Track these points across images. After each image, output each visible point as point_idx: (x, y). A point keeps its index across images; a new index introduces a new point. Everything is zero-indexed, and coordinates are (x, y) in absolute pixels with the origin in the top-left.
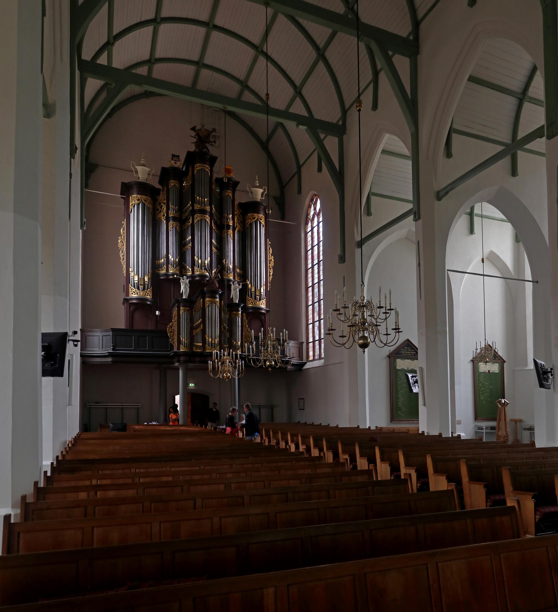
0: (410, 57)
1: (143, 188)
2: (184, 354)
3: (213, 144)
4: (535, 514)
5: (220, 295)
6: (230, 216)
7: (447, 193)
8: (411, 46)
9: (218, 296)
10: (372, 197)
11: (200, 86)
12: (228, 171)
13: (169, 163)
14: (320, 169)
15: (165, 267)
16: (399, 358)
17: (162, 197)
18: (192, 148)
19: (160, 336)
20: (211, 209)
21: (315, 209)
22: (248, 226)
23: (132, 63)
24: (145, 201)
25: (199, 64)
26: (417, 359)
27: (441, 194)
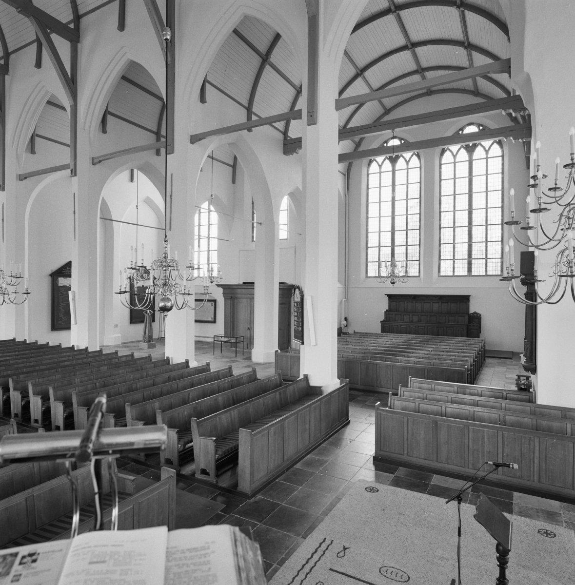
0: (71, 41)
7: (100, 162)
8: (74, 35)
10: (109, 116)
14: (38, 64)
16: (61, 277)
26: (381, 322)
27: (95, 161)
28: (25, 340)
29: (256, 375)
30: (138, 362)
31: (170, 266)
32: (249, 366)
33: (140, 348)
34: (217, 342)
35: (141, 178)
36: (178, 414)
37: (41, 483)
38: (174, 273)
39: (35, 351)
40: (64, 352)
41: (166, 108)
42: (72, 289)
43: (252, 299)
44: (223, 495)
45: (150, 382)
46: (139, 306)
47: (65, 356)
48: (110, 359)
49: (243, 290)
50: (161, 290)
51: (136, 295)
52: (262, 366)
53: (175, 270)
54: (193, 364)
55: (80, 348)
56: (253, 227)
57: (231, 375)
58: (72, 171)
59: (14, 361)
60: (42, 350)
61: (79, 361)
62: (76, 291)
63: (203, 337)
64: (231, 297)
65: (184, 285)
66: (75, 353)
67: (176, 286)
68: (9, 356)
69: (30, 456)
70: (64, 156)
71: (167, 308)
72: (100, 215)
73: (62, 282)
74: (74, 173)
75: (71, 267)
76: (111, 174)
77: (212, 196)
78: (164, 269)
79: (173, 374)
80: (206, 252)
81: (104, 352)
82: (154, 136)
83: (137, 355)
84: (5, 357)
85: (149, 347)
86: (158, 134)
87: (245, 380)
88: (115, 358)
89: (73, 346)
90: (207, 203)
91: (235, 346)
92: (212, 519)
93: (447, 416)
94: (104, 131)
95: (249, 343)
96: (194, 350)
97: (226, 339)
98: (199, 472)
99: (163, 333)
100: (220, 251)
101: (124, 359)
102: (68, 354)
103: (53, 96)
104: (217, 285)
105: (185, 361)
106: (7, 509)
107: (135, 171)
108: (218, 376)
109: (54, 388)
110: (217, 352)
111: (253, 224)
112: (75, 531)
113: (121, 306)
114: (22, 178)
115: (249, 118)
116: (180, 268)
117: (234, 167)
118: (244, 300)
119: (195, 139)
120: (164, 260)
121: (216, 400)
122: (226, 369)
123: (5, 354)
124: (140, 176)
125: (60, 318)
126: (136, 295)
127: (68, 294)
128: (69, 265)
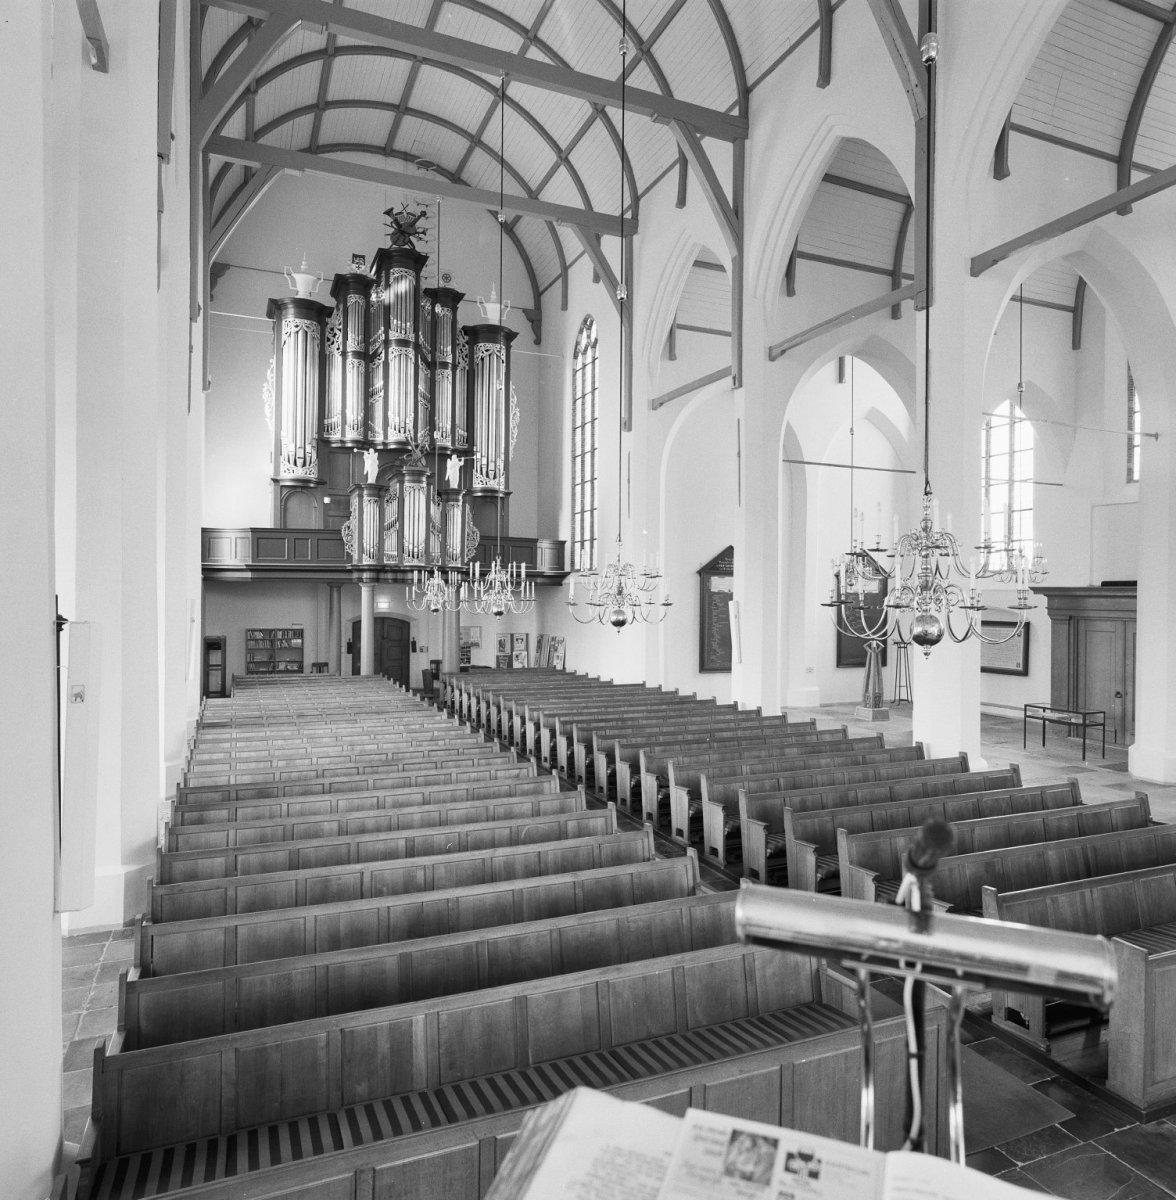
1: (310, 310)
2: (370, 569)
3: (421, 236)
4: (817, 872)
5: (428, 477)
6: (449, 348)
7: (783, 352)
8: (736, 127)
9: (424, 479)
11: (400, 144)
12: (447, 278)
13: (349, 268)
15: (340, 428)
17: (336, 321)
18: (387, 244)
19: (331, 536)
20: (417, 337)
21: (589, 337)
22: (479, 361)
23: (287, 110)
24: (307, 327)
25: (402, 109)
28: (660, 686)
29: (1147, 812)
30: (856, 746)
31: (938, 547)
32: (1121, 786)
33: (855, 717)
34: (1032, 720)
35: (860, 370)
36: (951, 870)
37: (692, 948)
38: (946, 563)
39: (676, 707)
40: (719, 714)
41: (915, 211)
42: (735, 597)
43: (1129, 619)
44: (1065, 1087)
45: (884, 791)
46: (869, 633)
47: (723, 722)
48: (803, 735)
49: (1102, 600)
50: (917, 599)
51: (861, 608)
52: (1160, 790)
53: (947, 555)
54: (978, 765)
55: (748, 709)
56: (1131, 447)
57: (1077, 802)
58: (734, 378)
59: (645, 722)
60: (685, 706)
61: (747, 733)
62: (742, 602)
63: (995, 705)
64: (1071, 617)
65: (972, 587)
66: (740, 717)
67: (949, 590)
68: (638, 712)
69: (796, 941)
70: (720, 353)
71: (929, 637)
72: (783, 454)
73: (718, 584)
74: (738, 382)
75: (732, 557)
76: (802, 374)
77: (1020, 385)
78: (924, 553)
79: (933, 781)
80: (1014, 516)
81: (791, 720)
82: (887, 280)
83: (855, 732)
84: (633, 712)
85: (875, 718)
86: (895, 274)
87: (1116, 818)
88: (810, 734)
89: (736, 703)
90: (1007, 403)
91: (1081, 733)
92: (1039, 1134)
93: (876, 826)
94: (790, 291)
95: (1119, 729)
96: (979, 733)
97: (1055, 716)
98: (1002, 1014)
99: (903, 690)
100: (1040, 509)
101: (828, 738)
102: (728, 717)
103: (704, 250)
104: (1032, 588)
105: (957, 755)
106: (645, 978)
107: (848, 359)
108: (1039, 800)
109: (708, 778)
110: (1034, 743)
111: (1130, 439)
112: (867, 1128)
113: (821, 629)
114: (657, 404)
115: (1123, 180)
116: (959, 551)
117: (1077, 311)
118: (1107, 626)
119: (980, 265)
120: (923, 534)
121: (1041, 855)
122: (1063, 786)
123: (632, 709)
124: (858, 368)
125: (714, 653)
126: (861, 608)
127: (727, 606)
128: (729, 552)
